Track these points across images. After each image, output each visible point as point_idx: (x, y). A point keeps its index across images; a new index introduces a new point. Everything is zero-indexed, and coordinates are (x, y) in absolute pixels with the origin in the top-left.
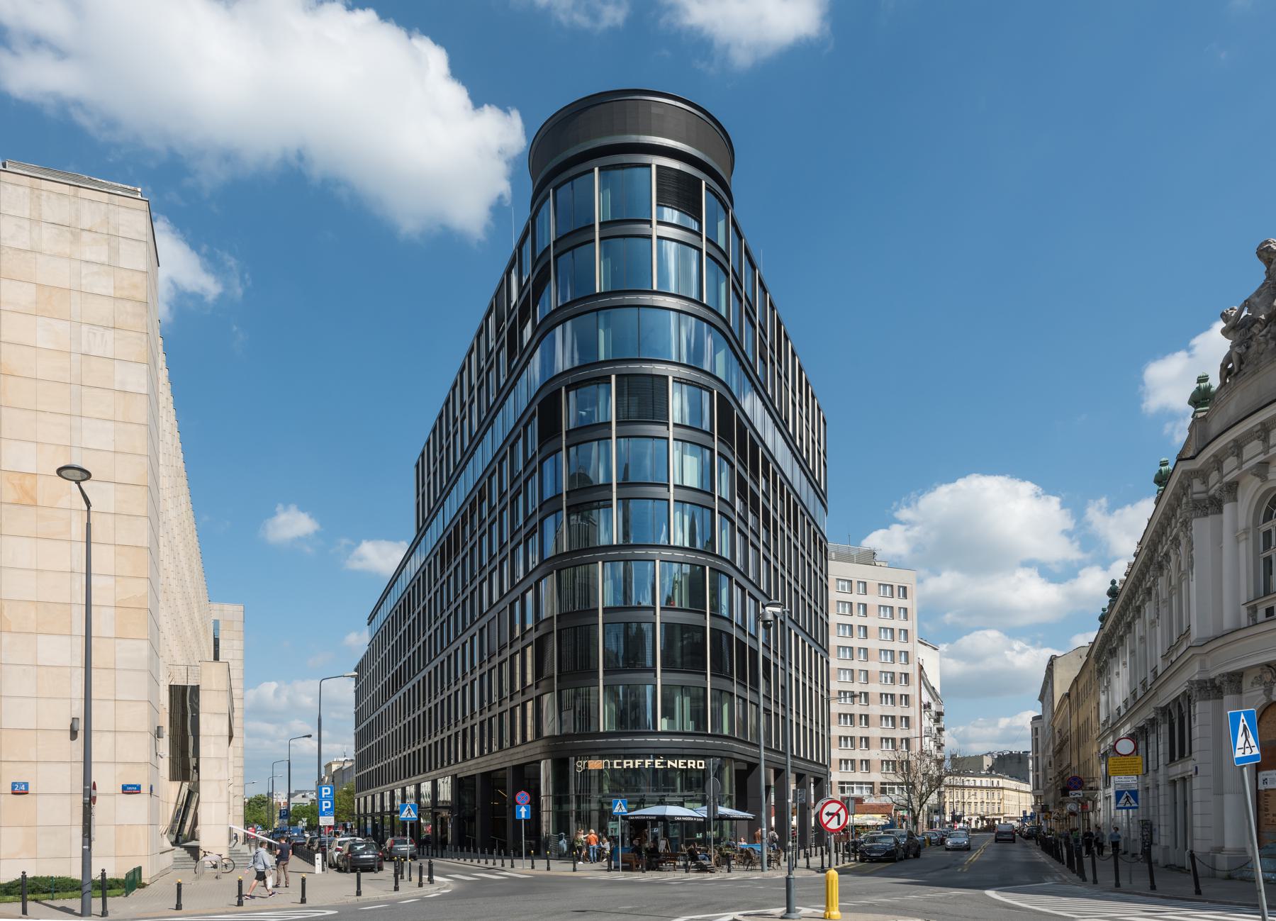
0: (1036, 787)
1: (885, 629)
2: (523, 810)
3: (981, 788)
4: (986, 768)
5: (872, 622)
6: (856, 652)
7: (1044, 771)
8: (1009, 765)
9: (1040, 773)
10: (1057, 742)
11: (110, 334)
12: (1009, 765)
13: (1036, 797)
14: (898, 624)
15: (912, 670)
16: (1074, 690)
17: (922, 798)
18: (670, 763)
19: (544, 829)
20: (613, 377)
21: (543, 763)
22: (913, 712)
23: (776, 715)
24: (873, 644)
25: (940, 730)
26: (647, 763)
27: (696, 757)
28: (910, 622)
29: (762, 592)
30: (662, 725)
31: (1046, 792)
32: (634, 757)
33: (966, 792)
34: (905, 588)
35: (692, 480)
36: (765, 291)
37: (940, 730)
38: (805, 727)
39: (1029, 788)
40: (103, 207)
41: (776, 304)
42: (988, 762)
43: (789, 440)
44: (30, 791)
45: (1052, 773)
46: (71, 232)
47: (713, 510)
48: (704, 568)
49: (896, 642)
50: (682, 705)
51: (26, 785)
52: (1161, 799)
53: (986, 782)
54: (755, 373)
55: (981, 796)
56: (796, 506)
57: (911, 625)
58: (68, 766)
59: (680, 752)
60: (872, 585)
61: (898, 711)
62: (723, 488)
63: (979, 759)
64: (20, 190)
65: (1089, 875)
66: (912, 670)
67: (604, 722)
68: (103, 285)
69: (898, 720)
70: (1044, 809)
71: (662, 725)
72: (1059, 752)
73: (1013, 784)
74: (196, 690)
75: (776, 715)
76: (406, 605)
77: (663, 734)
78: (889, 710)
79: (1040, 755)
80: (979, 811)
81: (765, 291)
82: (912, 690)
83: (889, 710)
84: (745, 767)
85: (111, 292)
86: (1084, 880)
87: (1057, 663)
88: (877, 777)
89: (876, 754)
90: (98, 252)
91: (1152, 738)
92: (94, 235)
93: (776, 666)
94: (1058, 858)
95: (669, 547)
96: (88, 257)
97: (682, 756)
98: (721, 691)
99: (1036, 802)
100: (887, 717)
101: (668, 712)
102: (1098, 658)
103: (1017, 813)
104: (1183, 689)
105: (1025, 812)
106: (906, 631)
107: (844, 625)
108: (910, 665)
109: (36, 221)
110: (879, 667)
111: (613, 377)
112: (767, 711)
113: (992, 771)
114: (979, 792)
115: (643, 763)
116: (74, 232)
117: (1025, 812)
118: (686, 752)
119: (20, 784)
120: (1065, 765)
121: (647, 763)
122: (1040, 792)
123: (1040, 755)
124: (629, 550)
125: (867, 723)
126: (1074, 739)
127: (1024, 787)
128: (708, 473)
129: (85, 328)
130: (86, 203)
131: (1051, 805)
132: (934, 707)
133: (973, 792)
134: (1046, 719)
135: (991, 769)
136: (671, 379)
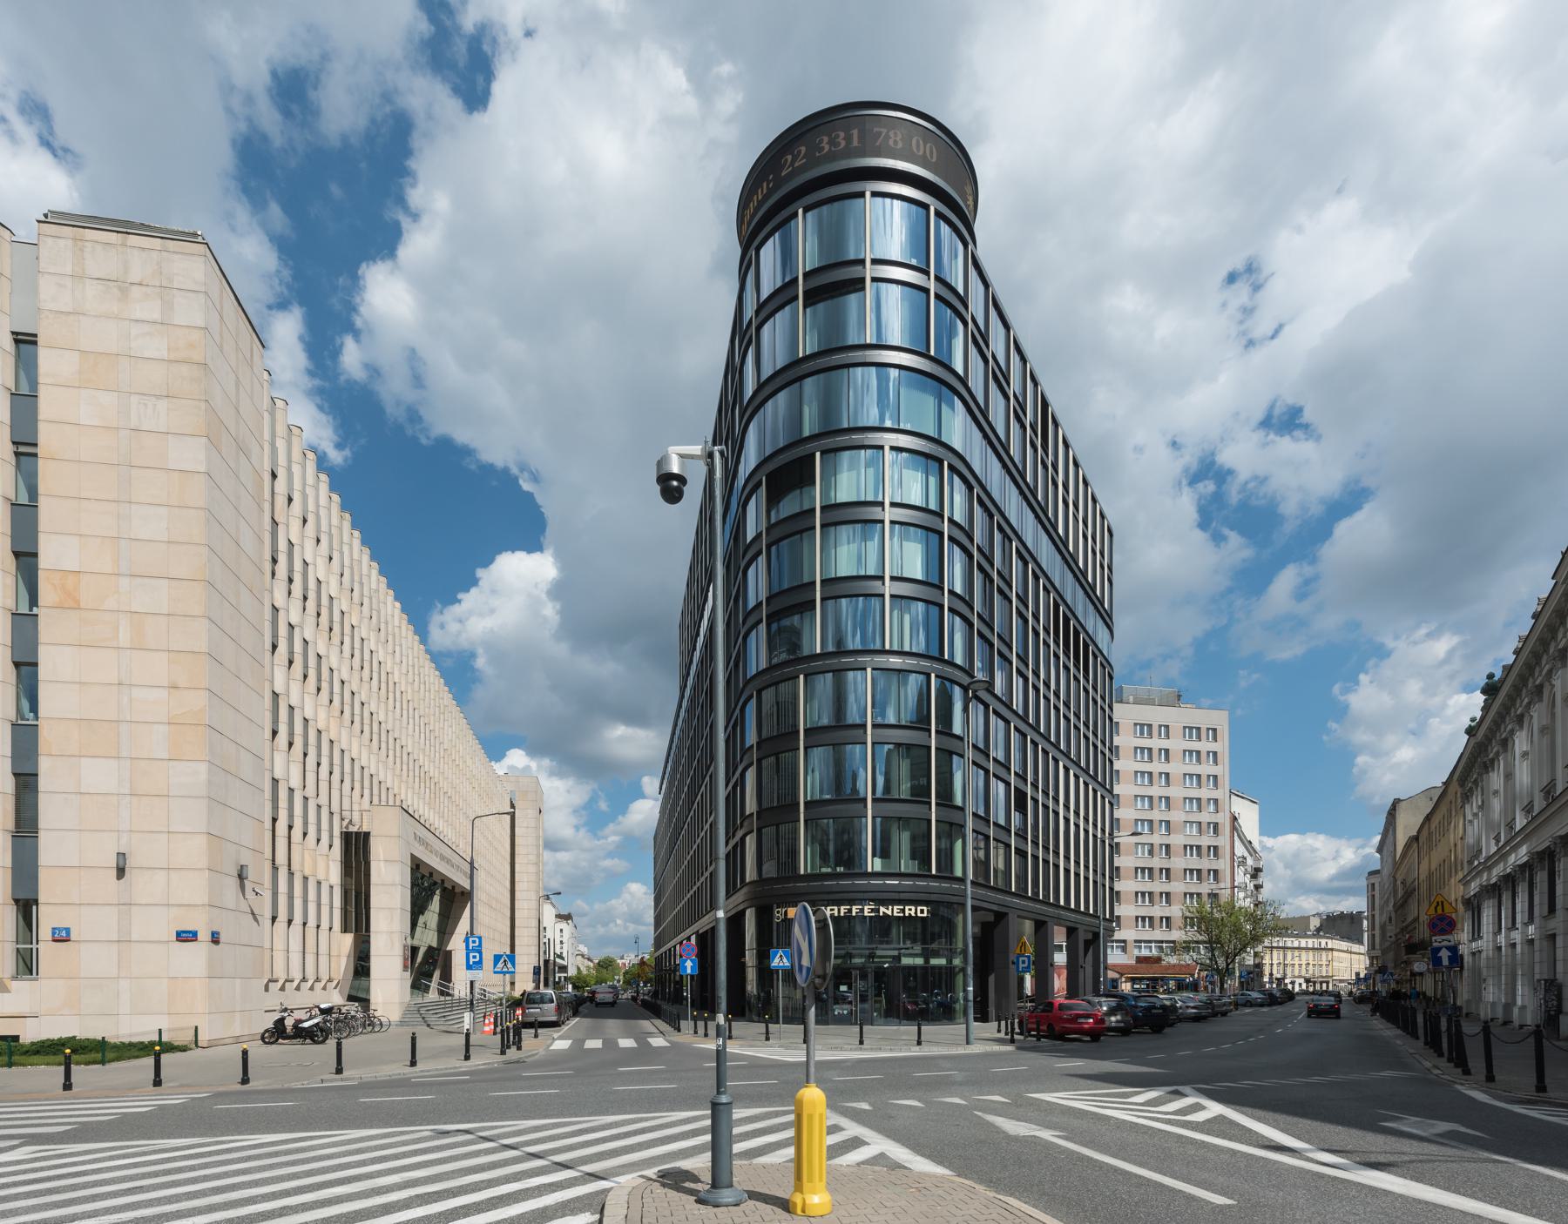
0: (1372, 946)
1: (1191, 775)
2: (689, 964)
3: (1307, 949)
4: (1312, 928)
5: (1176, 768)
6: (1156, 801)
7: (1383, 928)
8: (1340, 926)
9: (1377, 932)
10: (1400, 893)
11: (163, 405)
12: (1340, 926)
13: (1372, 958)
14: (1206, 769)
15: (1223, 819)
16: (1425, 832)
17: (1230, 957)
18: (882, 909)
19: (749, 988)
20: (818, 454)
21: (748, 912)
22: (1223, 865)
23: (1035, 858)
24: (1176, 792)
25: (1258, 887)
26: (855, 910)
27: (916, 903)
28: (1220, 767)
29: (1015, 713)
30: (874, 864)
31: (1384, 952)
32: (839, 903)
33: (1289, 954)
34: (1215, 730)
35: (916, 570)
36: (1024, 360)
37: (1258, 887)
38: (1077, 875)
39: (1363, 949)
40: (155, 255)
41: (1098, 497)
42: (1315, 923)
43: (1059, 544)
44: (73, 937)
45: (1392, 930)
46: (120, 289)
47: (941, 607)
48: (928, 676)
49: (1204, 789)
50: (902, 841)
51: (68, 930)
52: (1537, 954)
53: (1311, 943)
54: (1024, 480)
55: (1306, 957)
56: (1067, 620)
57: (1222, 770)
58: (115, 909)
59: (895, 896)
60: (1176, 729)
61: (1205, 864)
62: (955, 577)
63: (1305, 920)
64: (62, 242)
65: (1476, 1063)
66: (1223, 819)
67: (805, 863)
68: (156, 347)
69: (1205, 874)
70: (1382, 970)
71: (874, 864)
72: (1401, 906)
73: (1344, 945)
74: (367, 835)
75: (1035, 858)
76: (676, 763)
77: (875, 875)
78: (1194, 862)
79: (1377, 913)
80: (1303, 973)
81: (1024, 360)
82: (1223, 841)
83: (1194, 862)
84: (991, 918)
85: (165, 355)
86: (1467, 1072)
87: (1401, 808)
88: (1177, 935)
89: (1176, 911)
90: (149, 309)
91: (1506, 897)
92: (143, 289)
93: (1035, 801)
94: (1409, 1028)
95: (883, 652)
96: (138, 315)
97: (899, 902)
98: (951, 824)
99: (1372, 964)
100: (1191, 871)
101: (883, 852)
102: (1462, 781)
103: (1349, 976)
104: (1547, 844)
105: (1357, 974)
106: (1215, 777)
107: (1143, 773)
108: (1220, 814)
109: (78, 277)
110: (1183, 817)
111: (818, 454)
112: (1022, 853)
113: (1318, 933)
114: (1303, 953)
115: (850, 911)
116: (122, 286)
117: (1357, 974)
118: (903, 896)
119: (60, 930)
120: (1410, 919)
121: (855, 910)
122: (1377, 953)
123: (1377, 913)
124: (838, 661)
125: (1168, 877)
126: (1424, 888)
127: (1356, 948)
128: (936, 562)
129: (134, 399)
130: (136, 252)
131: (1390, 965)
132: (1250, 861)
133: (1296, 953)
134: (1385, 872)
135: (1318, 930)
136: (887, 448)
